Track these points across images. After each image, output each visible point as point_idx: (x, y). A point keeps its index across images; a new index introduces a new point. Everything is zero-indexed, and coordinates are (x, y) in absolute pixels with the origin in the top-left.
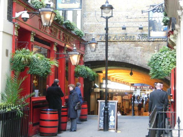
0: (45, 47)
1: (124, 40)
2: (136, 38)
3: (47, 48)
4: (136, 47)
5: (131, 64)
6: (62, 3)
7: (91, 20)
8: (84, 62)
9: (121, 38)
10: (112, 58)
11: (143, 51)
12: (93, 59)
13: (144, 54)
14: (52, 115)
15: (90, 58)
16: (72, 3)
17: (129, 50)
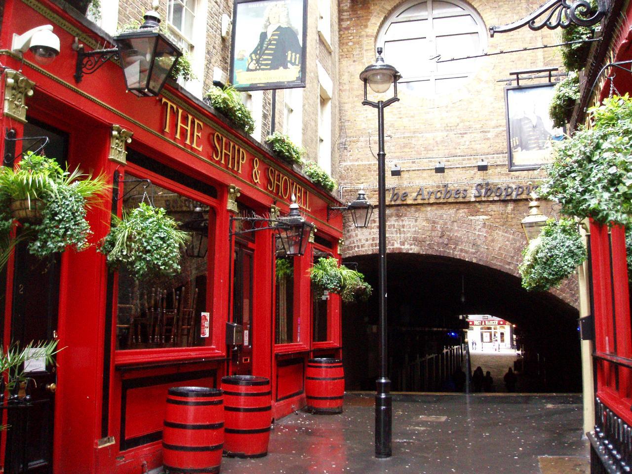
0: (161, 182)
1: (442, 201)
2: (472, 196)
3: (176, 189)
4: (472, 218)
5: (460, 260)
6: (249, 70)
7: (359, 156)
8: (343, 259)
9: (433, 197)
10: (411, 245)
11: (491, 227)
12: (363, 249)
13: (494, 233)
14: (202, 408)
15: (358, 247)
16: (278, 69)
17: (455, 224)
